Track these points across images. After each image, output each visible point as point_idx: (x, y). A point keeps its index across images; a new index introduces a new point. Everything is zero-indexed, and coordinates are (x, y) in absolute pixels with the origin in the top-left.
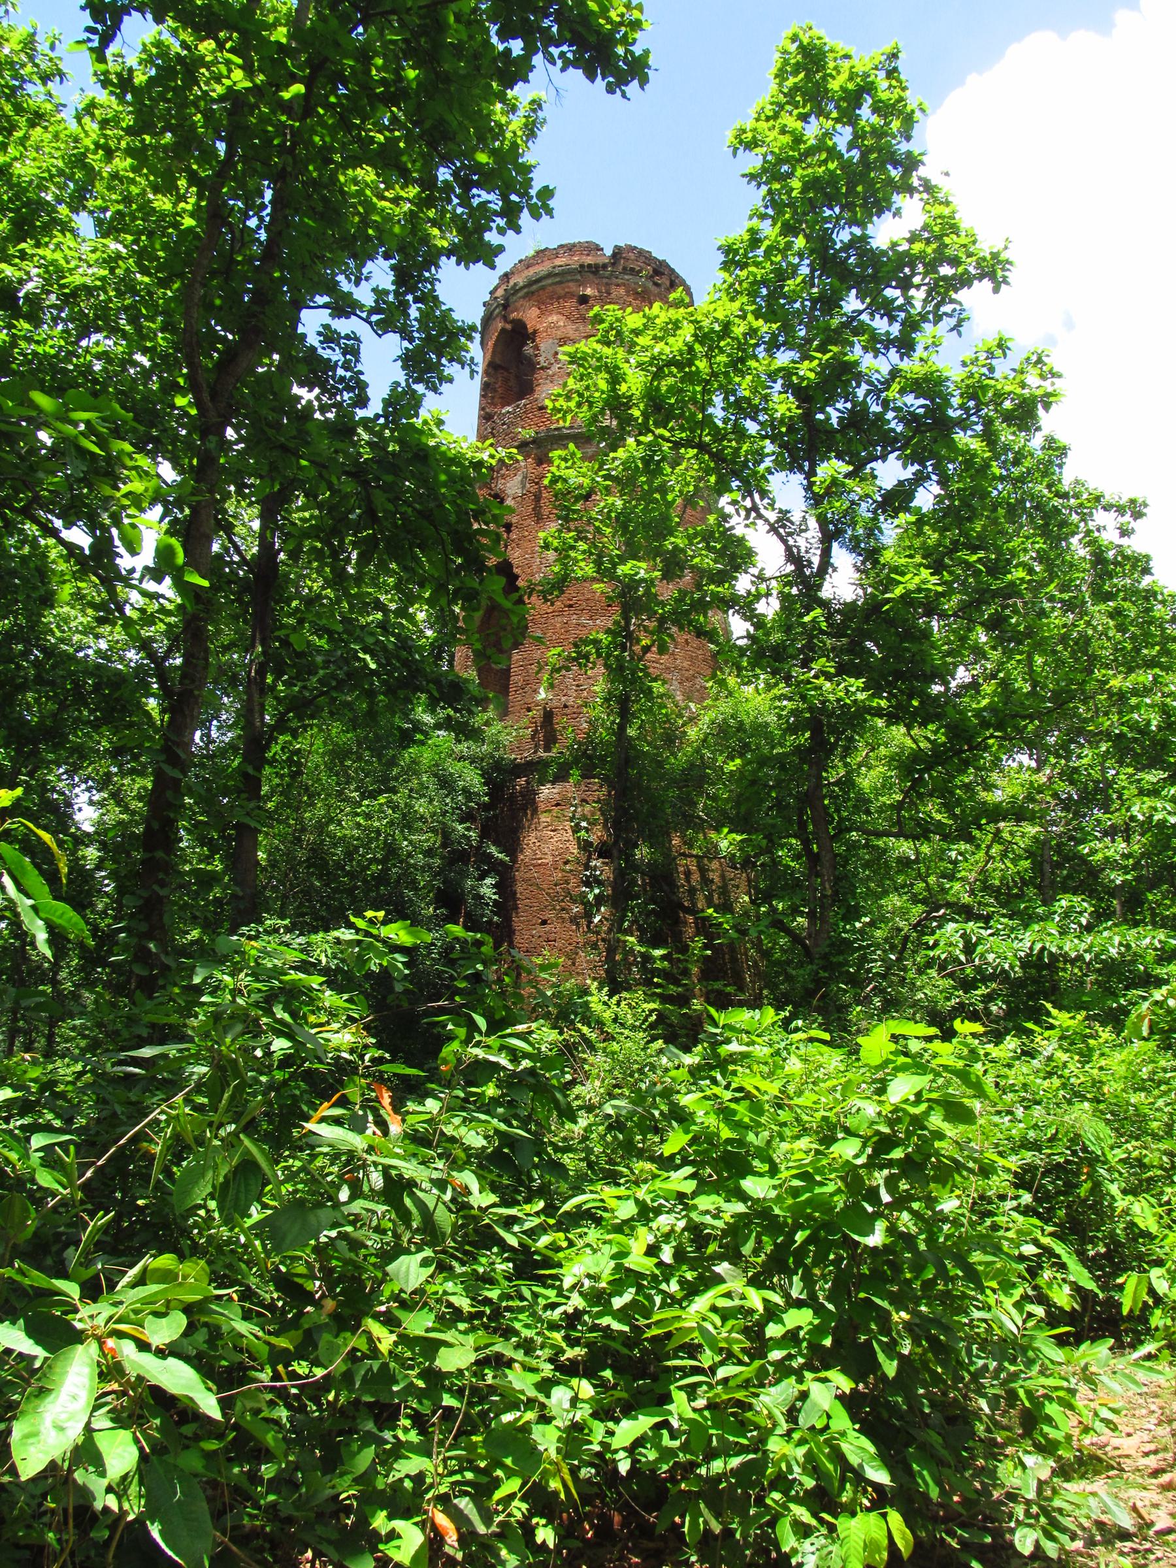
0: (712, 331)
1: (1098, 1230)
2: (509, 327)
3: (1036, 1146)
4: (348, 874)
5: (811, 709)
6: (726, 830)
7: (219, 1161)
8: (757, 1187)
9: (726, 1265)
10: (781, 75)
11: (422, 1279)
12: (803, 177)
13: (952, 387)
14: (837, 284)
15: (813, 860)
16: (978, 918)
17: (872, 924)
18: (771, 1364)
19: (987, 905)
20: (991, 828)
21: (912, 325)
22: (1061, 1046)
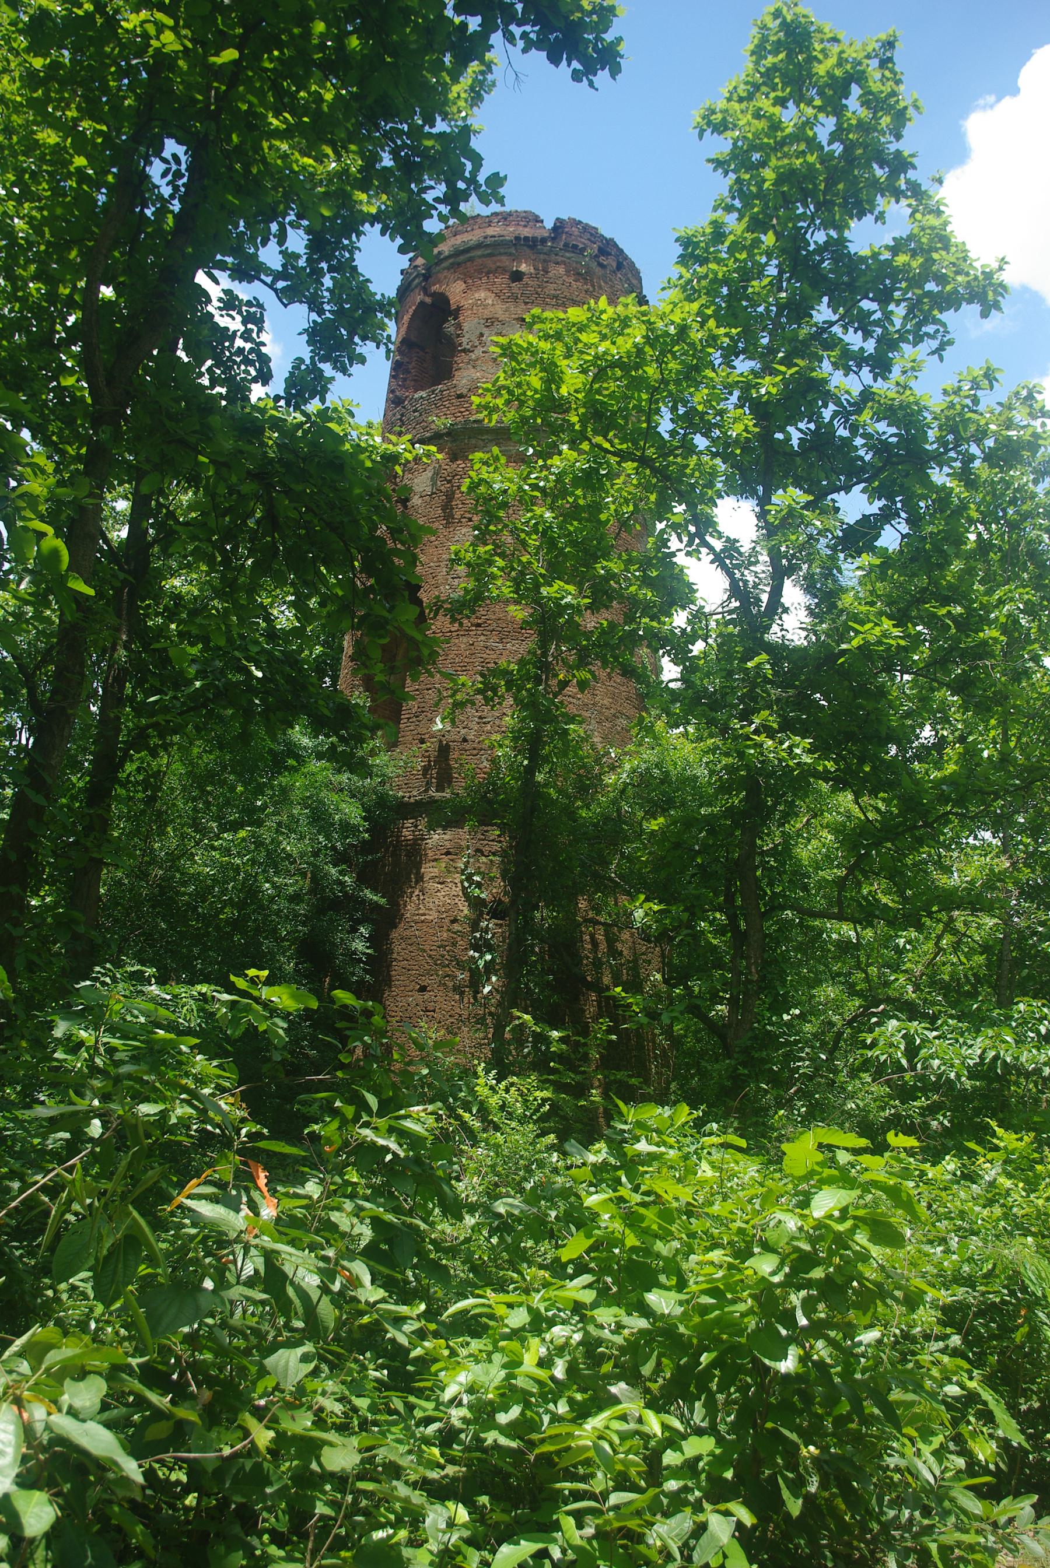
0: (667, 334)
1: (1033, 1382)
2: (428, 300)
3: (970, 1282)
4: (199, 917)
5: (748, 767)
6: (642, 897)
7: (104, 1232)
8: (661, 1301)
9: (622, 1385)
10: (759, 52)
11: (301, 1376)
12: (778, 168)
13: (929, 417)
14: (808, 290)
15: (740, 939)
16: (924, 1017)
17: (802, 1017)
18: (666, 1495)
19: (934, 1003)
20: (943, 916)
21: (888, 344)
22: (1004, 1171)
